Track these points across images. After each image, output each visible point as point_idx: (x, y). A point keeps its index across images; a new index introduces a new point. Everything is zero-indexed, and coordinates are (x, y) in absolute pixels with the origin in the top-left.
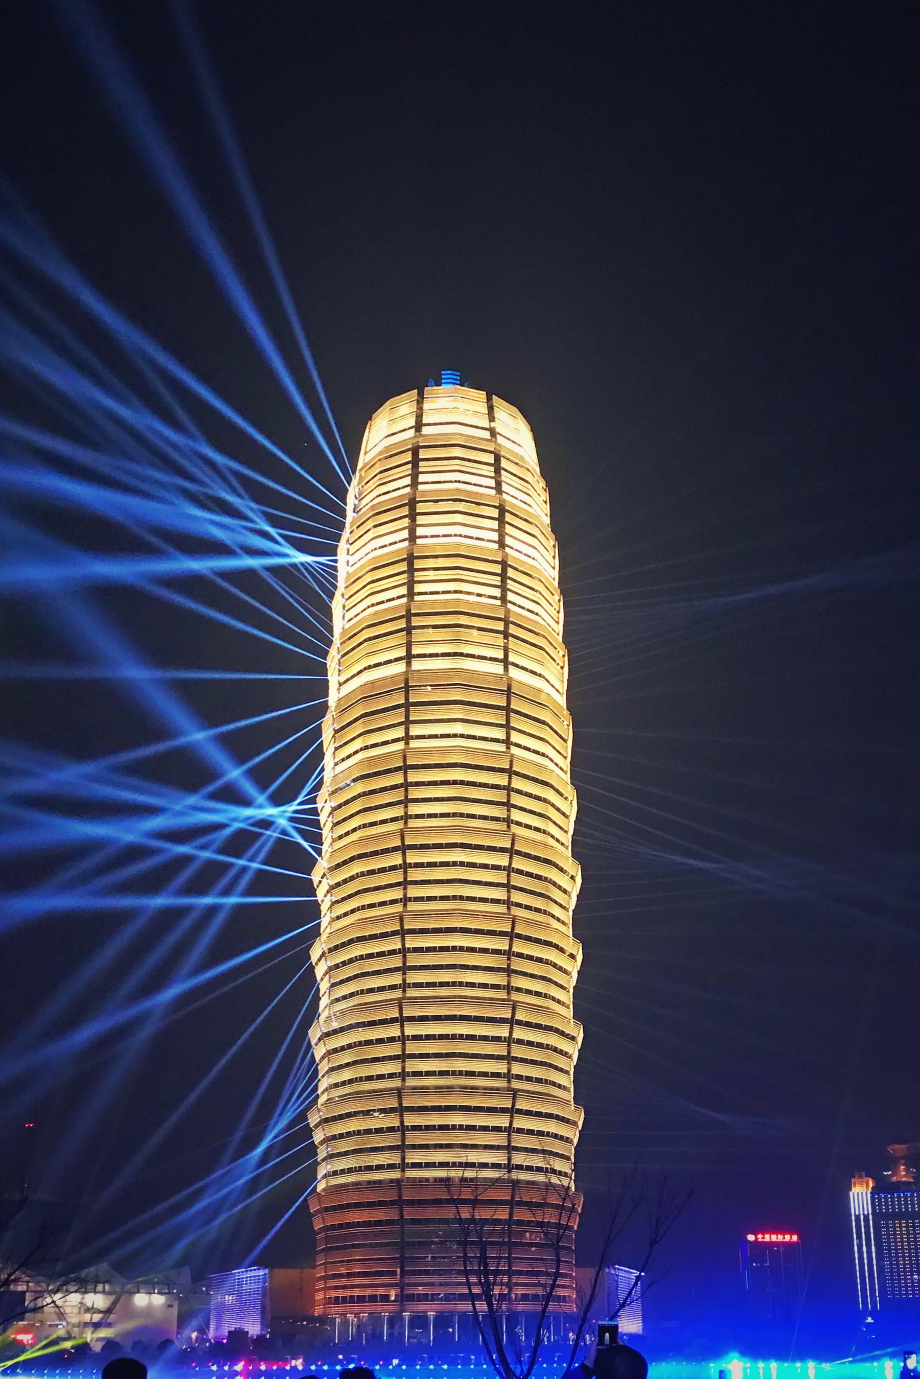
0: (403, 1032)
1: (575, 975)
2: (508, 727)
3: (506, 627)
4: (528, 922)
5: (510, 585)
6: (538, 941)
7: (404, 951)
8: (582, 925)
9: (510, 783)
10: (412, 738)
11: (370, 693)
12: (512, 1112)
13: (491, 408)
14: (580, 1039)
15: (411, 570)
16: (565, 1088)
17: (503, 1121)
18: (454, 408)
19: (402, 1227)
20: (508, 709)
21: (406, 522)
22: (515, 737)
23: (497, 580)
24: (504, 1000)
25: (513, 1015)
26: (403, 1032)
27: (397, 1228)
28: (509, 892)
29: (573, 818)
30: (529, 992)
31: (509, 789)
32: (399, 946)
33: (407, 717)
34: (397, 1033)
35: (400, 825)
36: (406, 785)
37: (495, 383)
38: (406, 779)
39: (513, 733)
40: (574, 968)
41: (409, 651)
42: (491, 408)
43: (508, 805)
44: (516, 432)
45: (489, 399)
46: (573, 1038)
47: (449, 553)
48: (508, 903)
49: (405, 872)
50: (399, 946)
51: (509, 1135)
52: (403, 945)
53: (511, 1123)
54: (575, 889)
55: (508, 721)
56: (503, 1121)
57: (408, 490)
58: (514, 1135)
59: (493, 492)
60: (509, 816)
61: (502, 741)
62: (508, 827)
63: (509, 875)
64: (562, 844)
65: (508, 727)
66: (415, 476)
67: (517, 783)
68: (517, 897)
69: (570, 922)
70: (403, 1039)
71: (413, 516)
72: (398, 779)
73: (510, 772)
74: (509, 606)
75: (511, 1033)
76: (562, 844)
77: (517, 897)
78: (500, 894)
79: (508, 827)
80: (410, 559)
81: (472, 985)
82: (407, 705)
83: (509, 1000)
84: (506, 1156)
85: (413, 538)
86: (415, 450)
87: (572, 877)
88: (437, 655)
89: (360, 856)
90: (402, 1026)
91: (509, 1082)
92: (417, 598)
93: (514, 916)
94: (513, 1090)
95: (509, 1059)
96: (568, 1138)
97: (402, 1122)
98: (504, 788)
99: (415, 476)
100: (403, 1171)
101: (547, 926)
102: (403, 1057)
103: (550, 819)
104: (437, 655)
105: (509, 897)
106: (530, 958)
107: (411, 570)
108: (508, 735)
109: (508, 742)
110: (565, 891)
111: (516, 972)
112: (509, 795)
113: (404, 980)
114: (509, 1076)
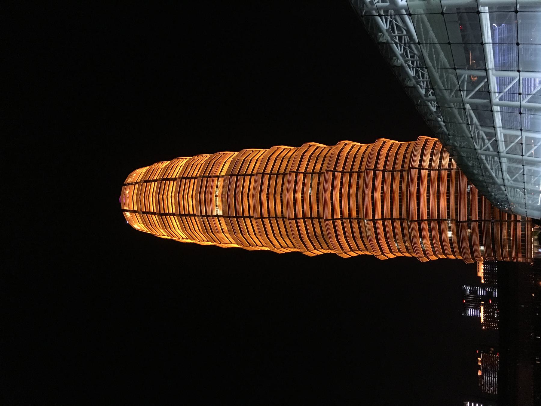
1: (393, 141)
2: (245, 175)
4: (328, 165)
5: (190, 175)
6: (378, 158)
8: (331, 142)
10: (249, 215)
11: (232, 231)
12: (375, 170)
13: (129, 184)
14: (385, 140)
15: (185, 215)
16: (409, 145)
17: (380, 174)
18: (129, 198)
19: (483, 220)
20: (238, 176)
21: (188, 218)
22: (249, 172)
23: (193, 181)
24: (408, 173)
25: (416, 168)
27: (483, 223)
28: (353, 172)
29: (318, 145)
30: (361, 163)
33: (241, 217)
34: (381, 222)
35: (322, 221)
37: (120, 183)
38: (267, 218)
39: (247, 173)
40: (390, 142)
42: (129, 184)
44: (139, 174)
45: (125, 185)
46: (384, 142)
51: (432, 170)
53: (426, 169)
54: (351, 143)
55: (243, 175)
56: (380, 174)
57: (175, 217)
58: (300, 171)
59: (156, 183)
60: (282, 174)
61: (251, 177)
62: (322, 173)
63: (346, 172)
64: (330, 149)
65: (245, 175)
66: (170, 214)
67: (268, 171)
68: (356, 168)
69: (367, 145)
71: (166, 214)
72: (267, 221)
74: (198, 175)
76: (330, 149)
77: (356, 168)
78: (355, 176)
79: (322, 173)
80: (181, 215)
81: (357, 189)
83: (408, 171)
84: (443, 171)
85: (173, 214)
86: (144, 213)
87: (346, 144)
89: (337, 238)
91: (405, 171)
92: (195, 213)
93: (366, 169)
94: (409, 169)
95: (393, 171)
96: (435, 143)
98: (270, 176)
99: (170, 214)
101: (370, 154)
102: (392, 219)
103: (397, 152)
105: (356, 172)
106: (403, 162)
107: (185, 215)
108: (248, 175)
109: (251, 175)
110: (352, 147)
111: (351, 169)
112: (309, 173)
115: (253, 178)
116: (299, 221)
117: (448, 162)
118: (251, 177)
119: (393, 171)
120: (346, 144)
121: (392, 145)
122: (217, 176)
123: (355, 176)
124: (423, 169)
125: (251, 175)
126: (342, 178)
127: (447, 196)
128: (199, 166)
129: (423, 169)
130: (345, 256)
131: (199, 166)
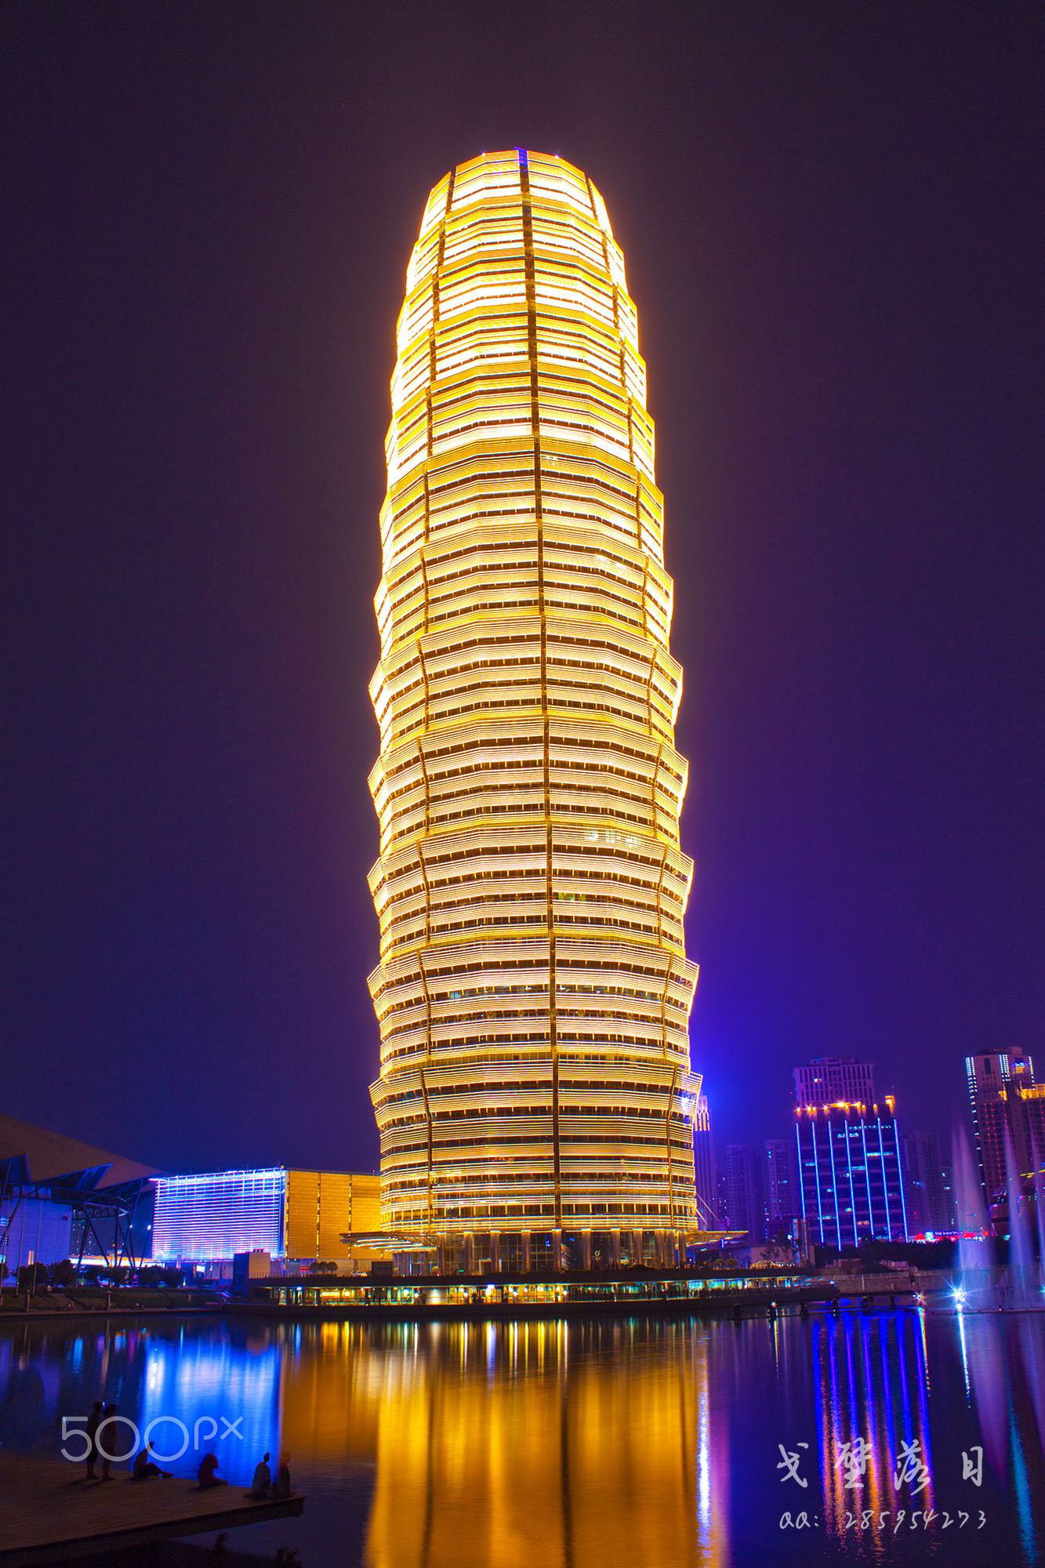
0: (549, 864)
2: (538, 494)
3: (534, 381)
7: (543, 661)
9: (540, 557)
26: (549, 864)
31: (540, 565)
32: (547, 1030)
36: (540, 565)
41: (535, 413)
43: (541, 584)
47: (517, 319)
48: (544, 702)
49: (546, 772)
50: (420, 776)
52: (543, 653)
56: (543, 978)
70: (546, 764)
73: (540, 545)
75: (546, 754)
78: (534, 693)
82: (537, 473)
88: (510, 421)
90: (544, 646)
95: (544, 681)
97: (553, 980)
100: (554, 1044)
104: (510, 421)
109: (539, 511)
113: (550, 912)
114: (547, 807)
115: (531, 518)
116: (422, 789)
117: (573, 915)
118: (533, 511)
119: (547, 786)
120: (673, 682)
121: (677, 898)
122: (535, 413)
123: (537, 798)
124: (553, 971)
125: (539, 511)
126: (527, 565)
127: (481, 920)
128: (647, 898)
129: (553, 971)
130: (374, 879)
131: (647, 898)
